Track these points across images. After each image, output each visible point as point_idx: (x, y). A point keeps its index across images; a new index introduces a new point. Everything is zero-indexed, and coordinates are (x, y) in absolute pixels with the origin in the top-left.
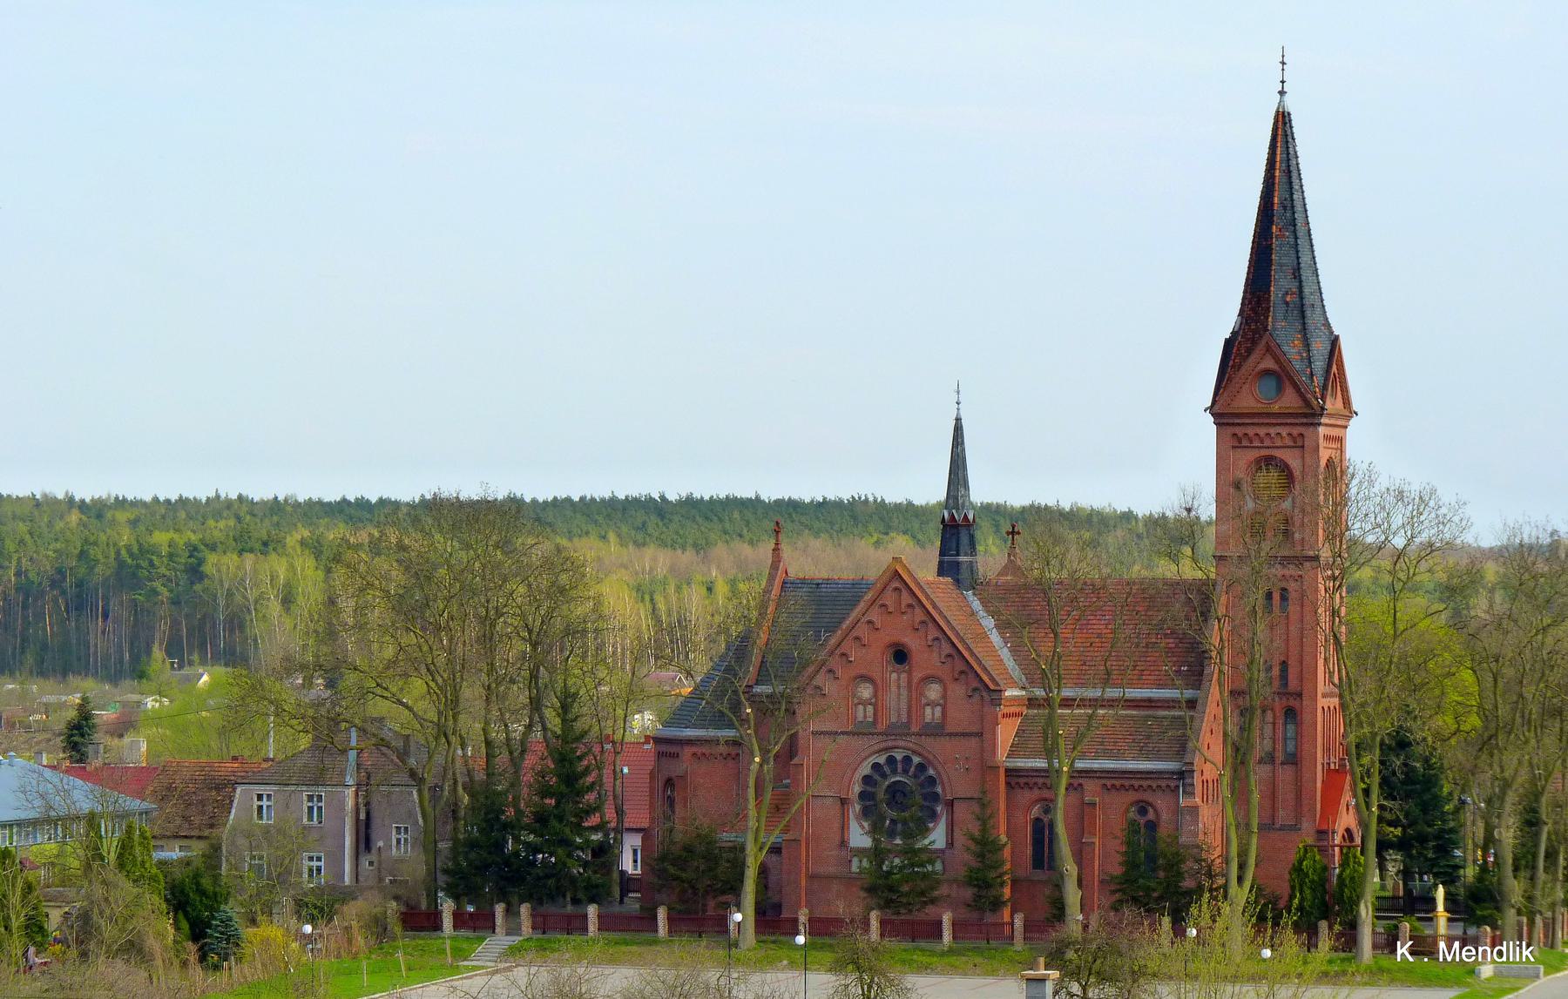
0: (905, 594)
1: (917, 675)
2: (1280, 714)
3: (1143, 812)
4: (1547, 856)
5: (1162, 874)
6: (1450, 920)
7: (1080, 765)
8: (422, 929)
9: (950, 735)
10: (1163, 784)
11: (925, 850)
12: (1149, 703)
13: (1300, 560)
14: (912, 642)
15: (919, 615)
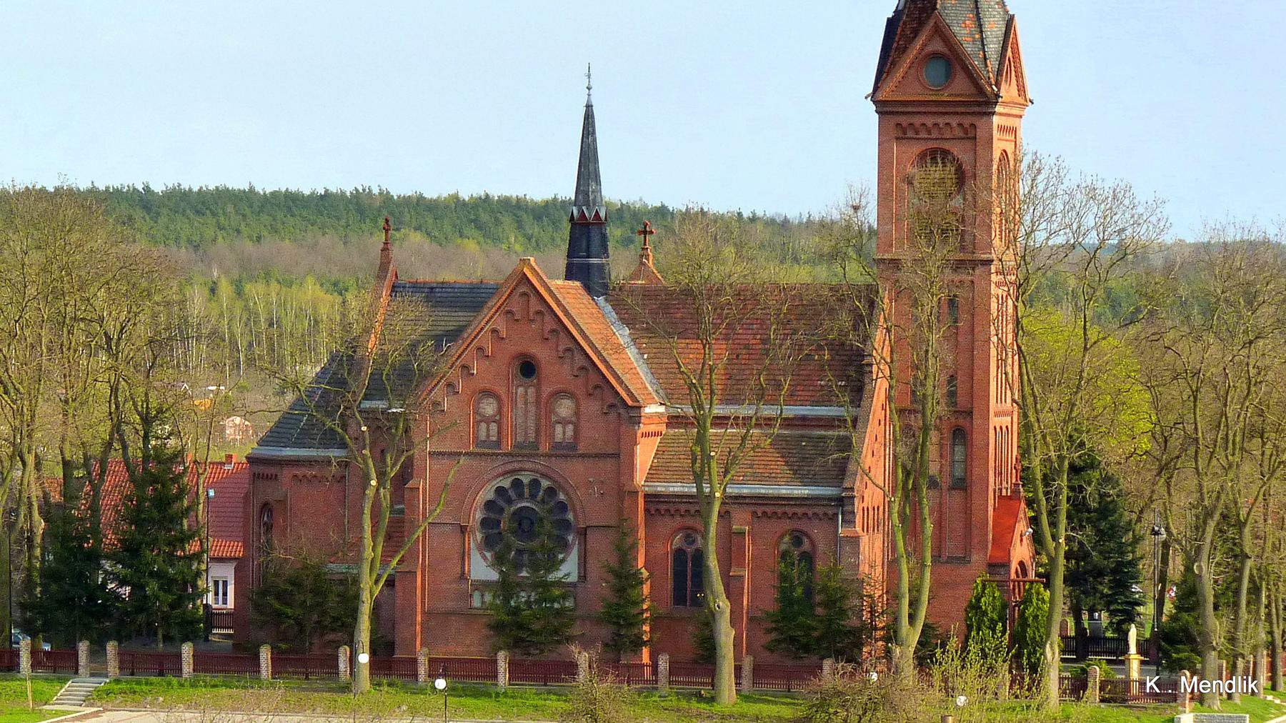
0: (533, 300)
1: (547, 390)
3: (797, 542)
5: (820, 611)
6: (1142, 663)
9: (583, 456)
10: (820, 510)
11: (558, 583)
12: (803, 421)
13: (975, 264)
14: (541, 353)
15: (550, 324)
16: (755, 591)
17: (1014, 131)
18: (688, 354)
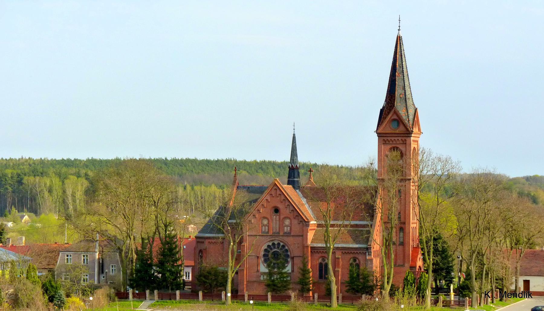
1: (282, 217)
2: (398, 229)
3: (355, 260)
4: (486, 275)
5: (361, 280)
6: (455, 295)
7: (336, 246)
8: (123, 298)
9: (293, 236)
10: (361, 252)
11: (285, 273)
12: (357, 226)
13: (406, 180)
14: (281, 206)
15: (283, 198)
16: (342, 275)
17: (417, 141)
18: (323, 206)
